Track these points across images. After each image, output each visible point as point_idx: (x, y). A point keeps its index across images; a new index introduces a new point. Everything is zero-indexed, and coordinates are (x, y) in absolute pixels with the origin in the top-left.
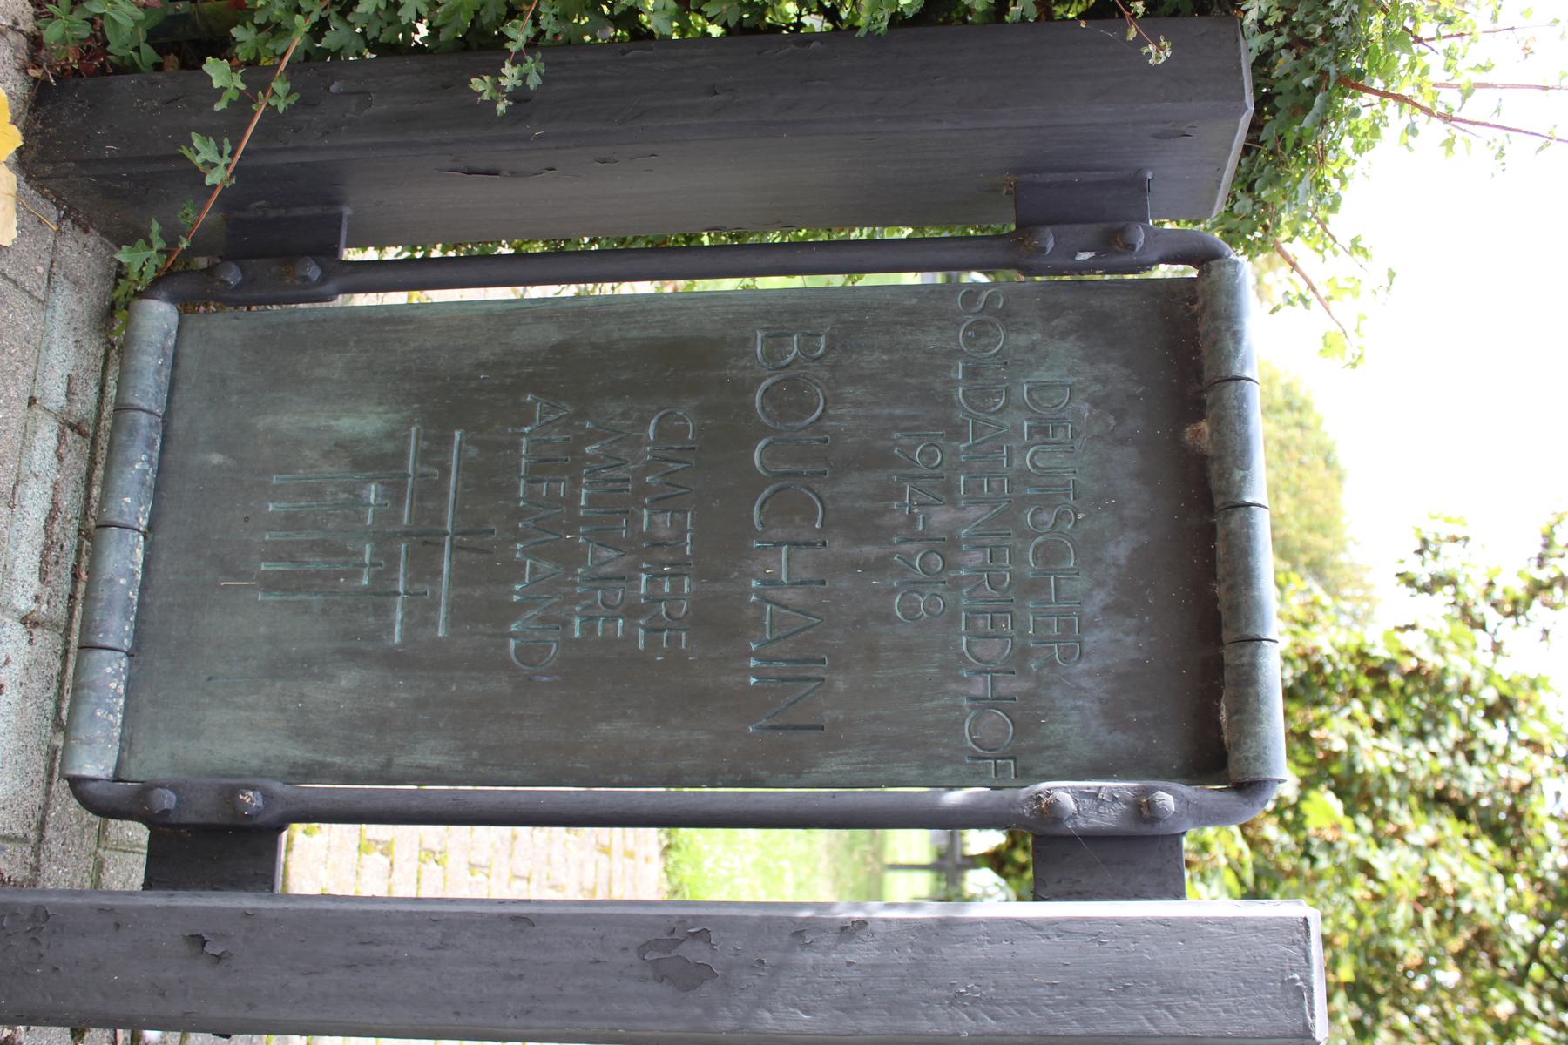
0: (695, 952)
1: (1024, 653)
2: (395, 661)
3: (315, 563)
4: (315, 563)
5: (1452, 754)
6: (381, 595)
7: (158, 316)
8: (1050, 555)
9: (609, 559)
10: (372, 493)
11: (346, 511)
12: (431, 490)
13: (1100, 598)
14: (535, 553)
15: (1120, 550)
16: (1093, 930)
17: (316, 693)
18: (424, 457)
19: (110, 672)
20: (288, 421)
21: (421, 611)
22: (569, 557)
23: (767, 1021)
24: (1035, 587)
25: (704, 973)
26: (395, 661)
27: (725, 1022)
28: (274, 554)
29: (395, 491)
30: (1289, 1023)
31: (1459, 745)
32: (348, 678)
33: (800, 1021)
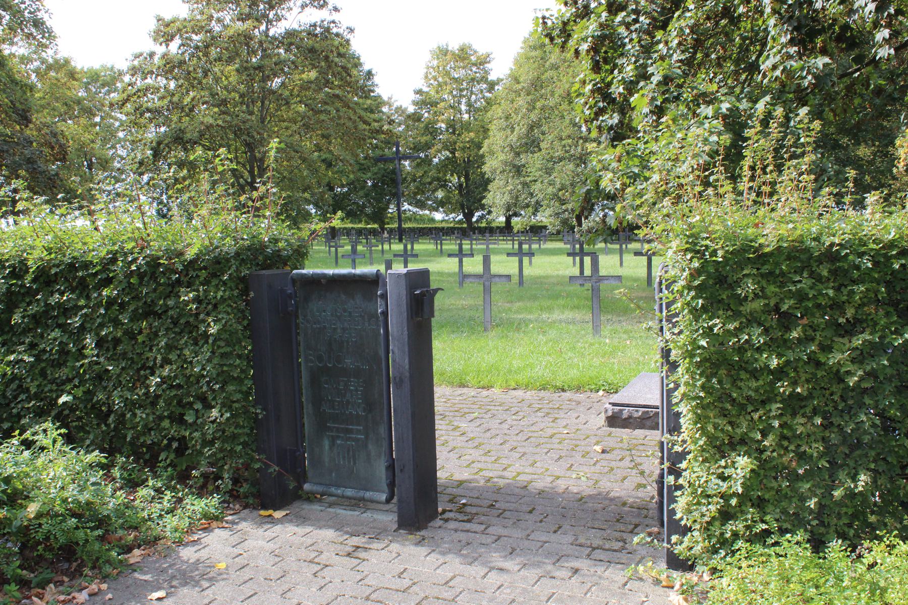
0: (397, 380)
1: (361, 316)
2: (367, 437)
3: (351, 453)
4: (351, 453)
5: (631, 32)
6: (357, 440)
7: (306, 487)
8: (345, 310)
9: (348, 395)
10: (339, 442)
11: (80, 313)
12: (338, 429)
13: (351, 301)
14: (348, 409)
15: (343, 297)
16: (392, 310)
17: (373, 453)
18: (332, 431)
19: (368, 495)
20: (327, 460)
21: (358, 432)
22: (348, 402)
23: (407, 367)
24: (350, 313)
25: (400, 378)
26: (367, 437)
27: (407, 374)
28: (349, 462)
29: (338, 437)
30: (403, 277)
31: (627, 28)
32: (370, 447)
33: (407, 361)
